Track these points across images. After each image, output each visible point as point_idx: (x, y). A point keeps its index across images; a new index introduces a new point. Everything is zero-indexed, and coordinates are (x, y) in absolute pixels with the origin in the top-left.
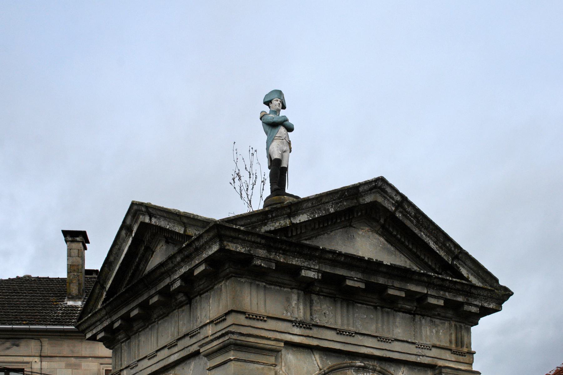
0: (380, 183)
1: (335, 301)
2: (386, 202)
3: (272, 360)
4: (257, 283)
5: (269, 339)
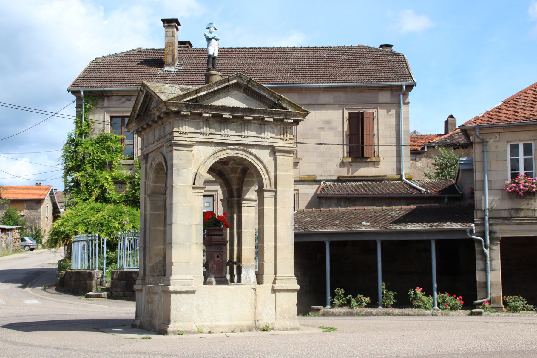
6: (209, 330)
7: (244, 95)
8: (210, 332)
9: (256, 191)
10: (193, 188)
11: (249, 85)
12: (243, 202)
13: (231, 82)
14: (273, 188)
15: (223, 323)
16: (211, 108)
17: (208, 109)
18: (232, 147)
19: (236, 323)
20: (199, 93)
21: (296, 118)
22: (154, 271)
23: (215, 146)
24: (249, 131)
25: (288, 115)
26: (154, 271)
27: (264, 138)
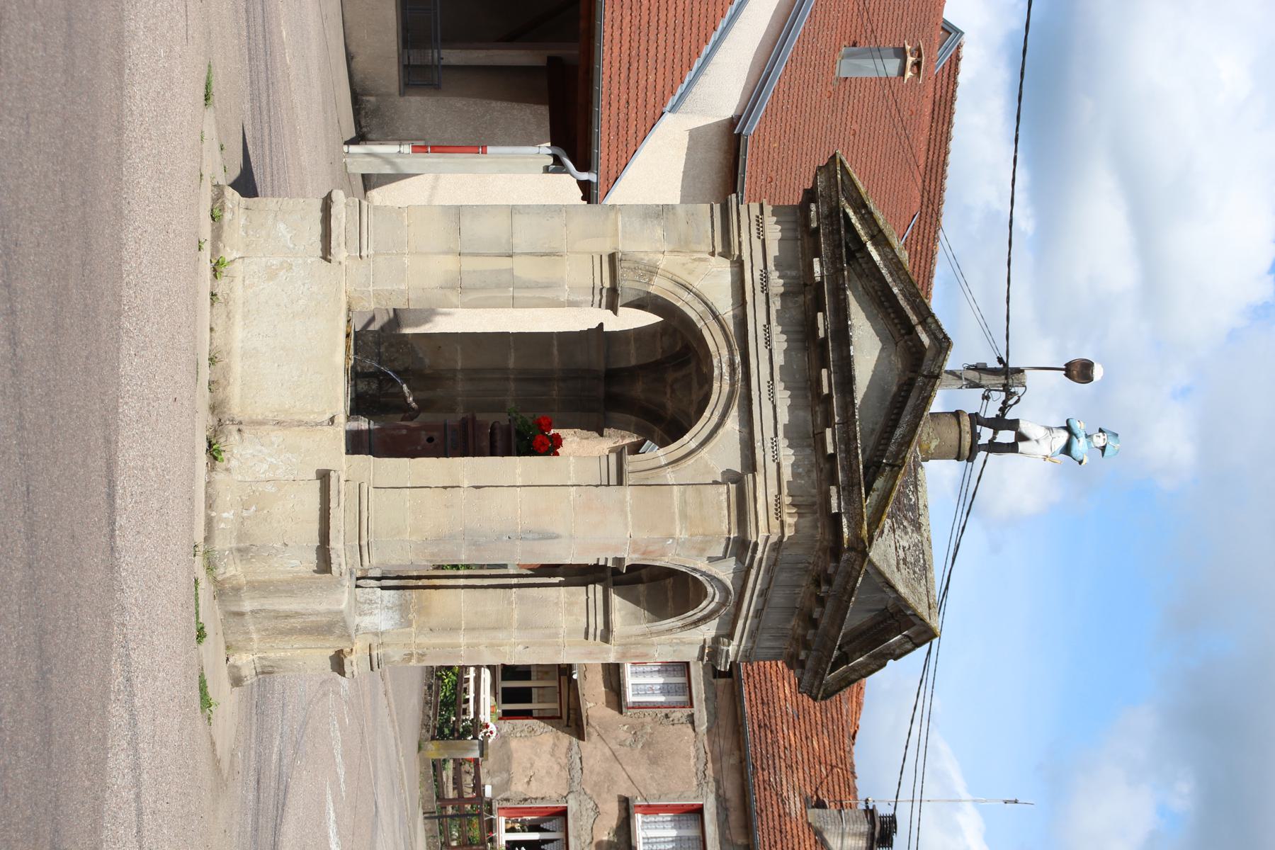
0: (945, 345)
3: (719, 249)
5: (739, 236)
6: (219, 296)
7: (894, 389)
9: (601, 325)
12: (599, 588)
13: (919, 329)
14: (629, 478)
15: (239, 333)
18: (738, 359)
19: (237, 368)
20: (874, 244)
21: (844, 521)
22: (391, 345)
23: (734, 316)
24: (789, 401)
25: (850, 492)
26: (391, 345)
27: (775, 444)
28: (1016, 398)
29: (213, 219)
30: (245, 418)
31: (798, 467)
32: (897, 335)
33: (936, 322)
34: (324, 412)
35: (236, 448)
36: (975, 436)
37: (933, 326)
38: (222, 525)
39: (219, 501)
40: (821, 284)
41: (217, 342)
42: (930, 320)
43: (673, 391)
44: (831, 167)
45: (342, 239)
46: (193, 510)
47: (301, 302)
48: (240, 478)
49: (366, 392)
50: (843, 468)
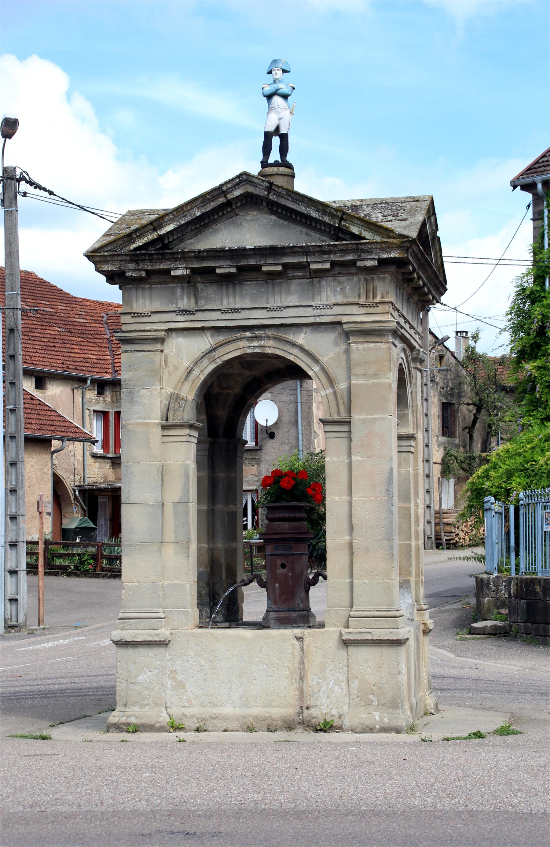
0: (245, 177)
1: (221, 284)
2: (257, 189)
3: (158, 346)
4: (142, 286)
5: (149, 331)
6: (198, 725)
7: (273, 217)
8: (198, 730)
10: (164, 427)
11: (272, 197)
14: (344, 416)
15: (228, 710)
16: (184, 256)
17: (180, 259)
18: (248, 334)
19: (257, 710)
21: (385, 256)
25: (363, 251)
27: (318, 307)
28: (24, 174)
29: (137, 731)
30: (297, 703)
31: (335, 290)
32: (231, 214)
33: (226, 183)
34: (293, 644)
35: (322, 708)
36: (276, 164)
37: (229, 186)
38: (386, 720)
39: (367, 723)
40: (193, 270)
41: (236, 726)
42: (224, 188)
43: (228, 388)
44: (97, 259)
45: (152, 632)
46: (217, 743)
47: (203, 663)
48: (346, 707)
49: (223, 614)
50: (342, 256)
